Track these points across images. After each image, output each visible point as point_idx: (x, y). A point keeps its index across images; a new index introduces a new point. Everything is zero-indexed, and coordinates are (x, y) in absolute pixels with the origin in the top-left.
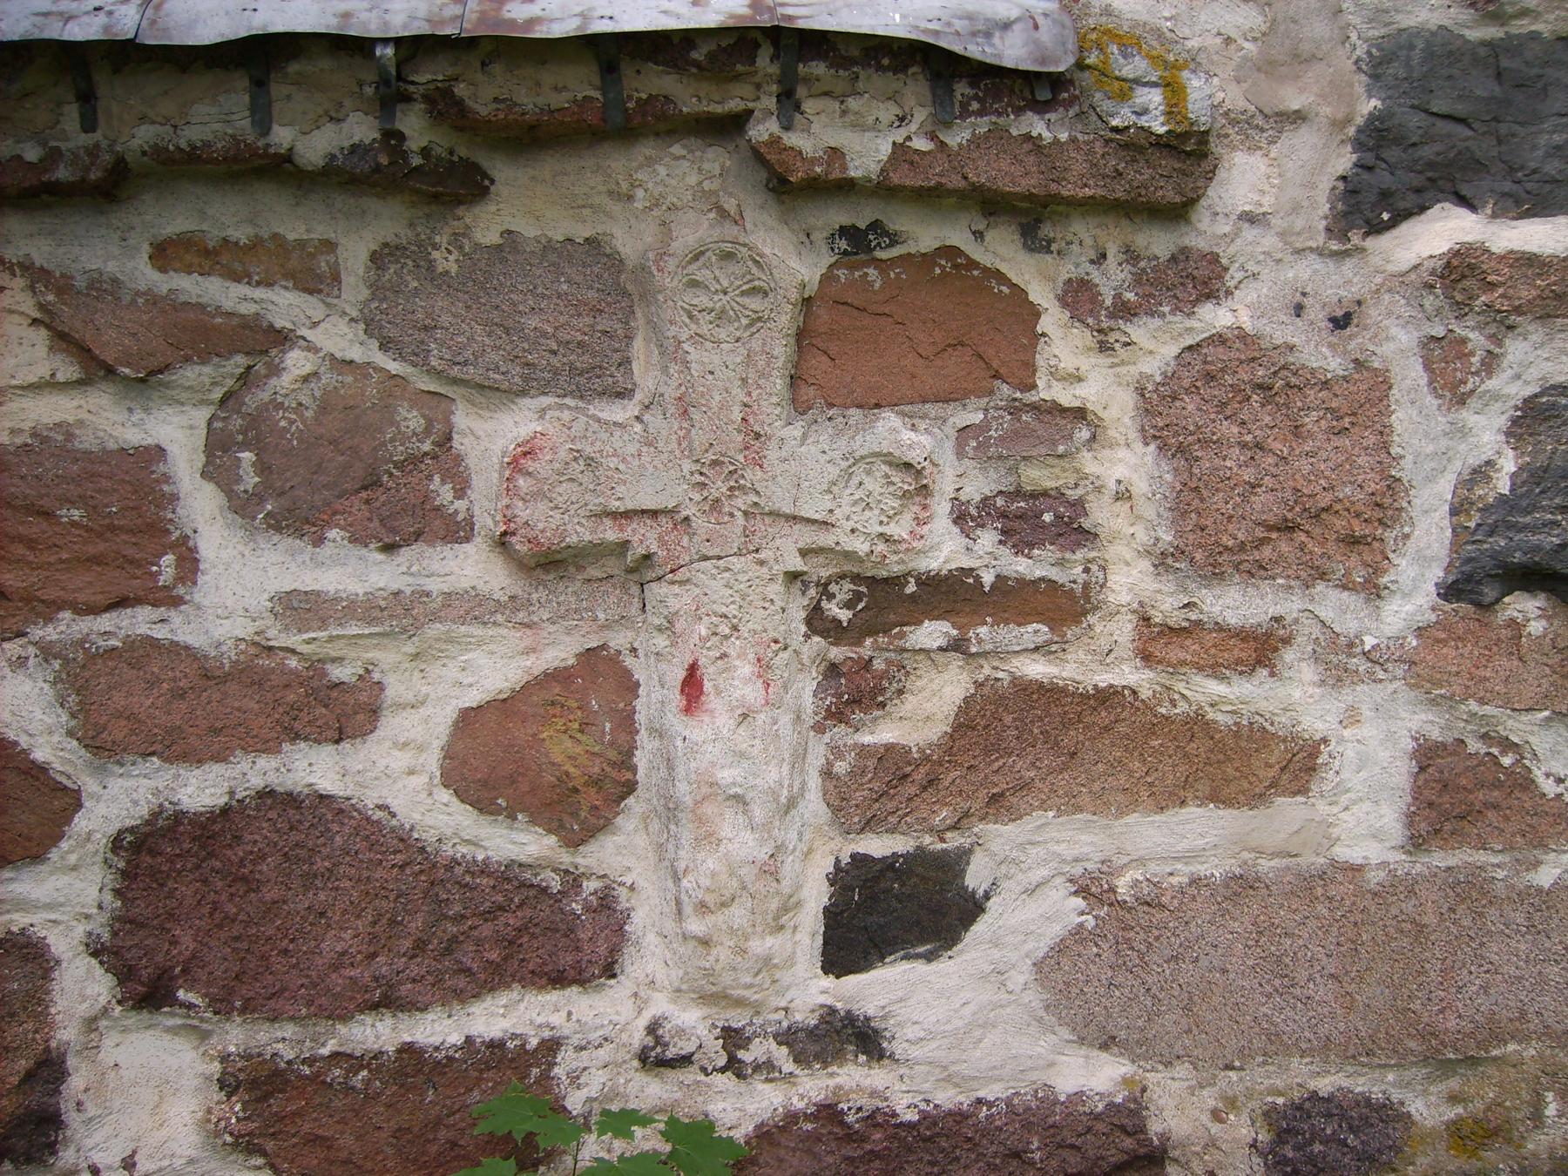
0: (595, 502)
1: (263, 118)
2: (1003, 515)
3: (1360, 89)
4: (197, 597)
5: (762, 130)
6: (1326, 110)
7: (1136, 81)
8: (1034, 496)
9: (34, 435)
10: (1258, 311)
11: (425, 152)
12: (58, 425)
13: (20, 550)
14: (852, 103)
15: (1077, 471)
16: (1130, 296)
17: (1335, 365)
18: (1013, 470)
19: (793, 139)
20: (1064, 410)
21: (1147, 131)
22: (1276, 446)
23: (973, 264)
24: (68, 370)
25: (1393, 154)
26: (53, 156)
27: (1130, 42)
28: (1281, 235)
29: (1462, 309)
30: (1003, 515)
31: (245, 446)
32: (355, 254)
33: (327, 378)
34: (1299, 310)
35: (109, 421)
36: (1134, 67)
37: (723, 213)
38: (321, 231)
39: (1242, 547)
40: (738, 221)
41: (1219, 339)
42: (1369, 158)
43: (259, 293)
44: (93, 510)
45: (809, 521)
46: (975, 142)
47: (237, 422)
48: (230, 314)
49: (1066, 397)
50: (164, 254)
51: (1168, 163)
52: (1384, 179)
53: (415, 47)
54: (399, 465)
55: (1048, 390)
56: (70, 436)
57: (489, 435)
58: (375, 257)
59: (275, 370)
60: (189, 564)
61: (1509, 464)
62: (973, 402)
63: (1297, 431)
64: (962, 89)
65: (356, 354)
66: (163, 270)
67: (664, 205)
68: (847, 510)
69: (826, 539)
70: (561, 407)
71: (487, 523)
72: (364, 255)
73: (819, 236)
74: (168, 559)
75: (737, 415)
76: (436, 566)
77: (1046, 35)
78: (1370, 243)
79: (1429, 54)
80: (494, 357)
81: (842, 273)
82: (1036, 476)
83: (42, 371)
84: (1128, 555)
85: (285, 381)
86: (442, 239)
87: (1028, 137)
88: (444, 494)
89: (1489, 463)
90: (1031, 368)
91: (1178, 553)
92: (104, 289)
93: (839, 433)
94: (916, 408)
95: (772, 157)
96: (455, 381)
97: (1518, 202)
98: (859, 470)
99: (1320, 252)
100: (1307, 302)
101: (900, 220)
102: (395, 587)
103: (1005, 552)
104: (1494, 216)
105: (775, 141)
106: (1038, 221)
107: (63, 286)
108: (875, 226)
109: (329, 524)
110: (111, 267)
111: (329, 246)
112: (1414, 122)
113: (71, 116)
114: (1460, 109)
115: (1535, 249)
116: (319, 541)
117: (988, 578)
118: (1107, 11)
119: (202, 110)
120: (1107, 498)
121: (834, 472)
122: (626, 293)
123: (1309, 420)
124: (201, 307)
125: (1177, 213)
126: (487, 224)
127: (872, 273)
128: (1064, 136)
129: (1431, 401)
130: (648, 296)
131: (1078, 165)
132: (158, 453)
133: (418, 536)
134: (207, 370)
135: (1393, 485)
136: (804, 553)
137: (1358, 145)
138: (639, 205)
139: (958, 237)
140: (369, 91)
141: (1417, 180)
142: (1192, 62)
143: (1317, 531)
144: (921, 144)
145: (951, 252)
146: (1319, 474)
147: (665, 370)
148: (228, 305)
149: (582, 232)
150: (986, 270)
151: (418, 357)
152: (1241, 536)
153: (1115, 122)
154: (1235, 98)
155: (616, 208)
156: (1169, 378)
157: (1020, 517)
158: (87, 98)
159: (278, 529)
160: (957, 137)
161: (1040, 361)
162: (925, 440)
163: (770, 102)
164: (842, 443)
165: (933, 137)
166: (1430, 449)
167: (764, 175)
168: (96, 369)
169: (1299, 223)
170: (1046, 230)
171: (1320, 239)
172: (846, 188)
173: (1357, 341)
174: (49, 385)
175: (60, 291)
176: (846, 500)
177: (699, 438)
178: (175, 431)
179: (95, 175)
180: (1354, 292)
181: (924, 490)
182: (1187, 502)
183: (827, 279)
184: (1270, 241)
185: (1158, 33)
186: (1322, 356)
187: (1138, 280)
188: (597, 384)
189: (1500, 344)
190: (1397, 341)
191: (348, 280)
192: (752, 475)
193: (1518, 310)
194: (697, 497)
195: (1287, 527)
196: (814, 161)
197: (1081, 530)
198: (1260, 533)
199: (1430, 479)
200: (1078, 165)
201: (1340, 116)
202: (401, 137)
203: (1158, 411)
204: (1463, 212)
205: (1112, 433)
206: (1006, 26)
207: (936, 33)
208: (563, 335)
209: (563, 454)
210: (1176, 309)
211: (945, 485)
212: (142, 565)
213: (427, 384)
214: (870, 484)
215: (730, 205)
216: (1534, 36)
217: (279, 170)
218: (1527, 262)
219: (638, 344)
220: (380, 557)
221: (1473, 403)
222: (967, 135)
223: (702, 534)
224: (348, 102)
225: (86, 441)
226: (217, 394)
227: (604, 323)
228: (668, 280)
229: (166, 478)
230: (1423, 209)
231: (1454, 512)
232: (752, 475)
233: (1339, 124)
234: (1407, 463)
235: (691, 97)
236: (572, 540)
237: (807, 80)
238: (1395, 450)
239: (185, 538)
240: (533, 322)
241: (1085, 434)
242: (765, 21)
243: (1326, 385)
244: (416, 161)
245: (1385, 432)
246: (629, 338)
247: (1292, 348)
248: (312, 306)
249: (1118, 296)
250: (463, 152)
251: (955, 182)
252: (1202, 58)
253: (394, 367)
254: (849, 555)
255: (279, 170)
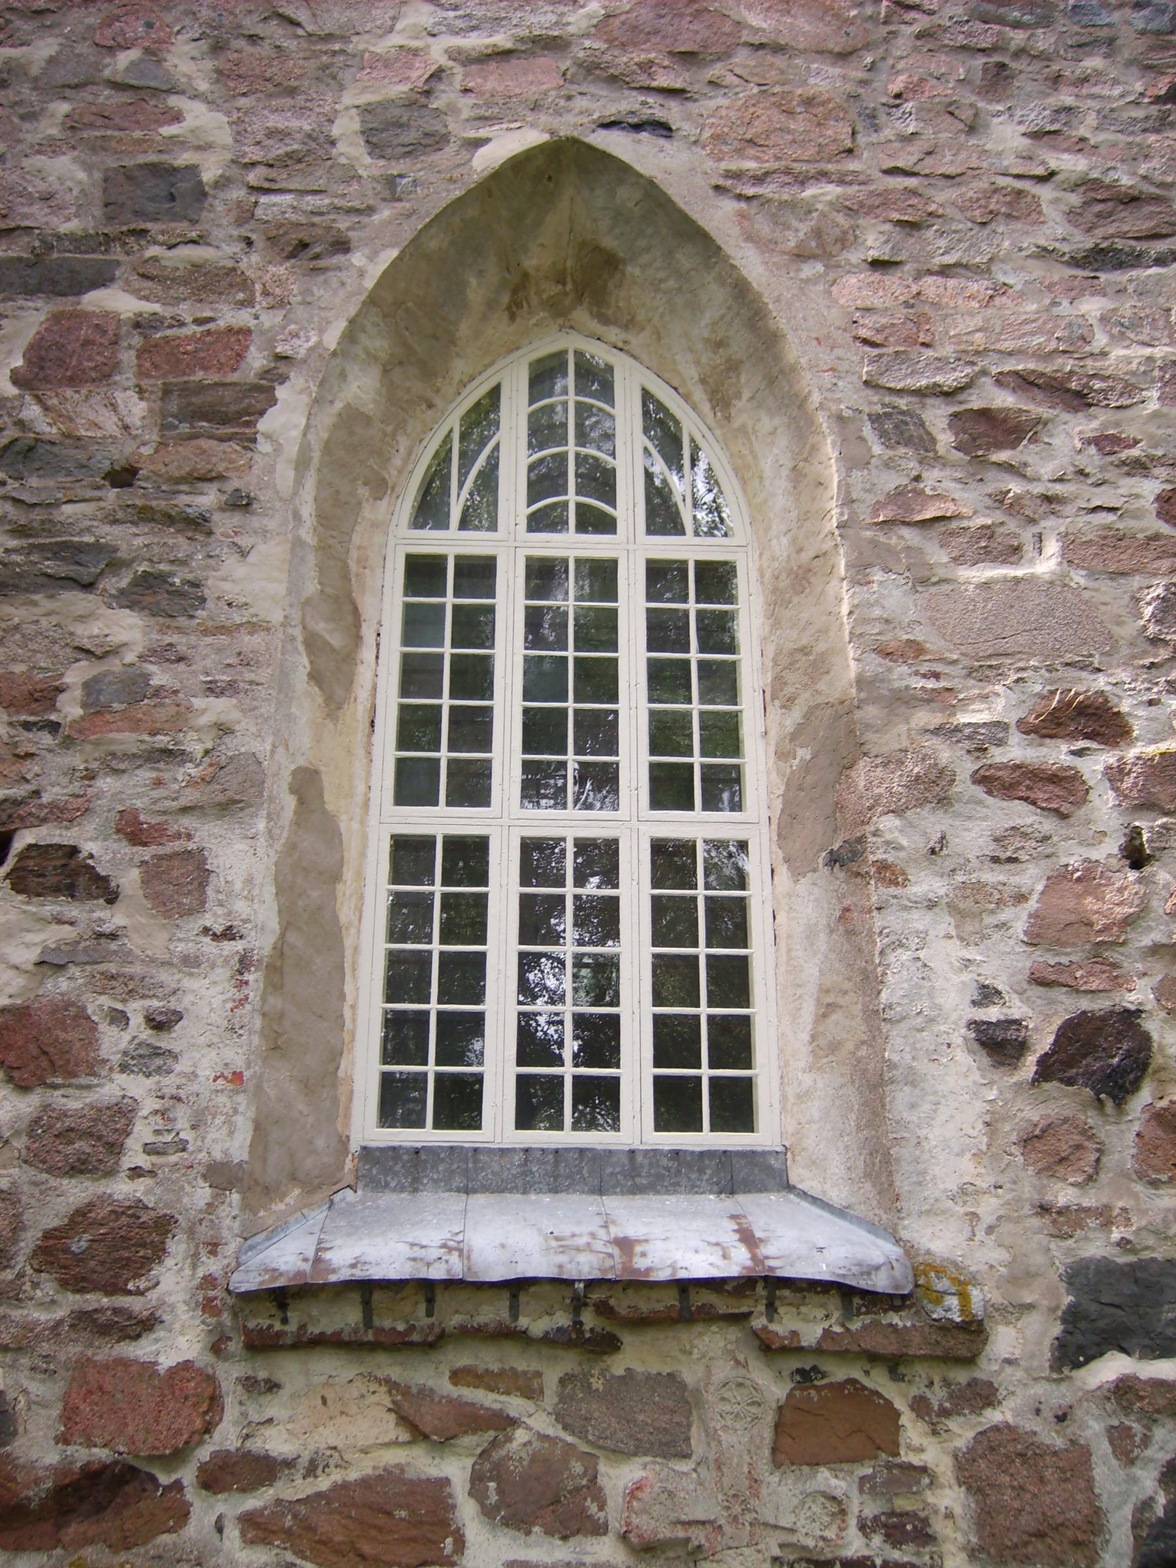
0: (673, 1516)
1: (515, 1312)
2: (885, 1526)
3: (1063, 1291)
4: (464, 1562)
5: (759, 1322)
6: (1045, 1302)
7: (945, 1293)
8: (901, 1515)
9: (385, 1470)
10: (1017, 1413)
11: (592, 1330)
12: (397, 1465)
13: (373, 1532)
14: (803, 1309)
15: (924, 1501)
16: (947, 1405)
17: (1059, 1443)
18: (890, 1500)
19: (773, 1327)
20: (914, 1468)
21: (951, 1320)
22: (1031, 1488)
23: (864, 1388)
24: (405, 1436)
25: (1083, 1325)
26: (412, 1328)
27: (940, 1271)
28: (1026, 1370)
29: (1127, 1410)
30: (885, 1526)
31: (491, 1479)
32: (551, 1377)
33: (536, 1444)
34: (1038, 1412)
35: (423, 1464)
36: (942, 1285)
37: (738, 1362)
38: (534, 1366)
39: (1016, 1546)
40: (745, 1366)
41: (996, 1428)
42: (1070, 1328)
43: (503, 1398)
44: (413, 1512)
45: (784, 1528)
46: (864, 1327)
47: (488, 1466)
48: (487, 1409)
49: (915, 1459)
50: (457, 1376)
51: (962, 1337)
52: (1079, 1338)
53: (590, 1284)
54: (570, 1492)
55: (907, 1457)
56: (402, 1471)
57: (619, 1477)
58: (562, 1381)
59: (509, 1439)
60: (460, 1544)
61: (1162, 1499)
62: (867, 1462)
63: (1042, 1479)
64: (857, 1301)
65: (550, 1432)
66: (455, 1384)
67: (708, 1358)
68: (803, 1522)
69: (793, 1539)
70: (654, 1463)
71: (615, 1525)
72: (556, 1380)
73: (786, 1373)
74: (449, 1540)
75: (746, 1470)
76: (588, 1549)
77: (898, 1272)
78: (1075, 1373)
79: (1098, 1272)
80: (620, 1435)
81: (797, 1393)
82: (903, 1504)
83: (392, 1436)
84: (954, 1550)
85: (514, 1445)
86: (595, 1372)
87: (891, 1325)
88: (593, 1508)
89: (1151, 1498)
90: (897, 1444)
91: (982, 1549)
92: (426, 1393)
93: (797, 1480)
94: (837, 1466)
95: (763, 1336)
96: (600, 1447)
97: (1153, 1351)
98: (809, 1499)
99: (1047, 1379)
100: (1042, 1407)
101: (827, 1365)
102: (567, 1560)
103: (887, 1547)
104: (1141, 1358)
105: (765, 1328)
106: (897, 1364)
107: (406, 1392)
108: (814, 1368)
109: (533, 1524)
110: (430, 1383)
111: (539, 1374)
112: (1093, 1308)
113: (422, 1308)
114: (1117, 1301)
115: (1164, 1377)
116: (528, 1533)
117: (878, 1562)
118: (928, 1252)
119: (485, 1308)
120: (940, 1517)
121: (795, 1501)
122: (687, 1402)
123: (1048, 1474)
124: (473, 1404)
125: (970, 1361)
126: (618, 1365)
127: (813, 1392)
128: (909, 1324)
129: (1114, 1462)
130: (700, 1404)
131: (917, 1338)
132: (446, 1482)
133: (578, 1531)
134: (475, 1438)
135: (1098, 1511)
136: (781, 1546)
137: (1064, 1320)
138: (695, 1356)
139: (856, 1374)
140: (568, 1301)
141: (1097, 1339)
142: (974, 1280)
143: (1057, 1537)
144: (837, 1329)
145: (853, 1382)
146: (1056, 1504)
147: (709, 1444)
148: (487, 1404)
149: (666, 1370)
150: (871, 1391)
151: (582, 1434)
152: (1015, 1540)
153: (935, 1316)
154: (996, 1297)
155: (683, 1358)
156: (971, 1450)
157: (894, 1526)
158: (430, 1301)
159: (507, 1525)
160: (855, 1325)
161: (902, 1441)
162: (843, 1484)
163: (762, 1308)
164: (800, 1486)
165: (843, 1325)
166: (1117, 1490)
167: (758, 1343)
168: (418, 1435)
169: (1035, 1364)
170: (902, 1370)
171: (1047, 1373)
172: (800, 1350)
173: (1071, 1429)
174: (395, 1443)
175: (403, 1395)
176: (802, 1517)
177: (726, 1481)
178: (455, 1469)
179: (430, 1339)
180: (1069, 1399)
181: (843, 1512)
182: (984, 1519)
183: (790, 1396)
184: (1020, 1374)
185: (955, 1263)
186: (1053, 1438)
187: (951, 1396)
188: (672, 1450)
189: (1150, 1430)
190: (1093, 1428)
191: (547, 1392)
192: (754, 1503)
193: (1158, 1411)
194: (725, 1514)
195: (1040, 1535)
196: (784, 1338)
197: (927, 1535)
198: (1025, 1538)
199: (1119, 1507)
200: (917, 1338)
201: (1053, 1305)
202: (581, 1324)
203: (967, 1468)
204: (1123, 1356)
205: (941, 1480)
206: (877, 1268)
207: (844, 1276)
208: (657, 1424)
209: (656, 1489)
210: (972, 1412)
211: (854, 1508)
212: (436, 1543)
213: (585, 1448)
214: (815, 1508)
215: (741, 1357)
216: (1153, 1260)
217: (522, 1337)
218: (1160, 1385)
219: (694, 1430)
220: (560, 1543)
221: (1138, 1463)
222: (860, 1324)
223: (729, 1534)
224: (556, 1306)
225: (410, 1474)
226: (479, 1451)
227: (676, 1419)
228: (710, 1397)
229: (450, 1496)
230: (1101, 1354)
231: (1135, 1526)
232: (754, 1503)
233: (1052, 1310)
234: (1105, 1497)
235: (723, 1306)
236: (661, 1536)
237: (781, 1298)
238: (1097, 1491)
239: (458, 1529)
240: (641, 1417)
241: (926, 1481)
242: (760, 1272)
243: (1055, 1453)
244: (588, 1335)
245: (1090, 1481)
246: (689, 1426)
247: (1035, 1433)
248: (529, 1406)
249: (941, 1405)
250: (608, 1329)
251: (855, 1348)
252: (978, 1276)
253: (569, 1439)
254: (805, 1548)
255: (522, 1337)
